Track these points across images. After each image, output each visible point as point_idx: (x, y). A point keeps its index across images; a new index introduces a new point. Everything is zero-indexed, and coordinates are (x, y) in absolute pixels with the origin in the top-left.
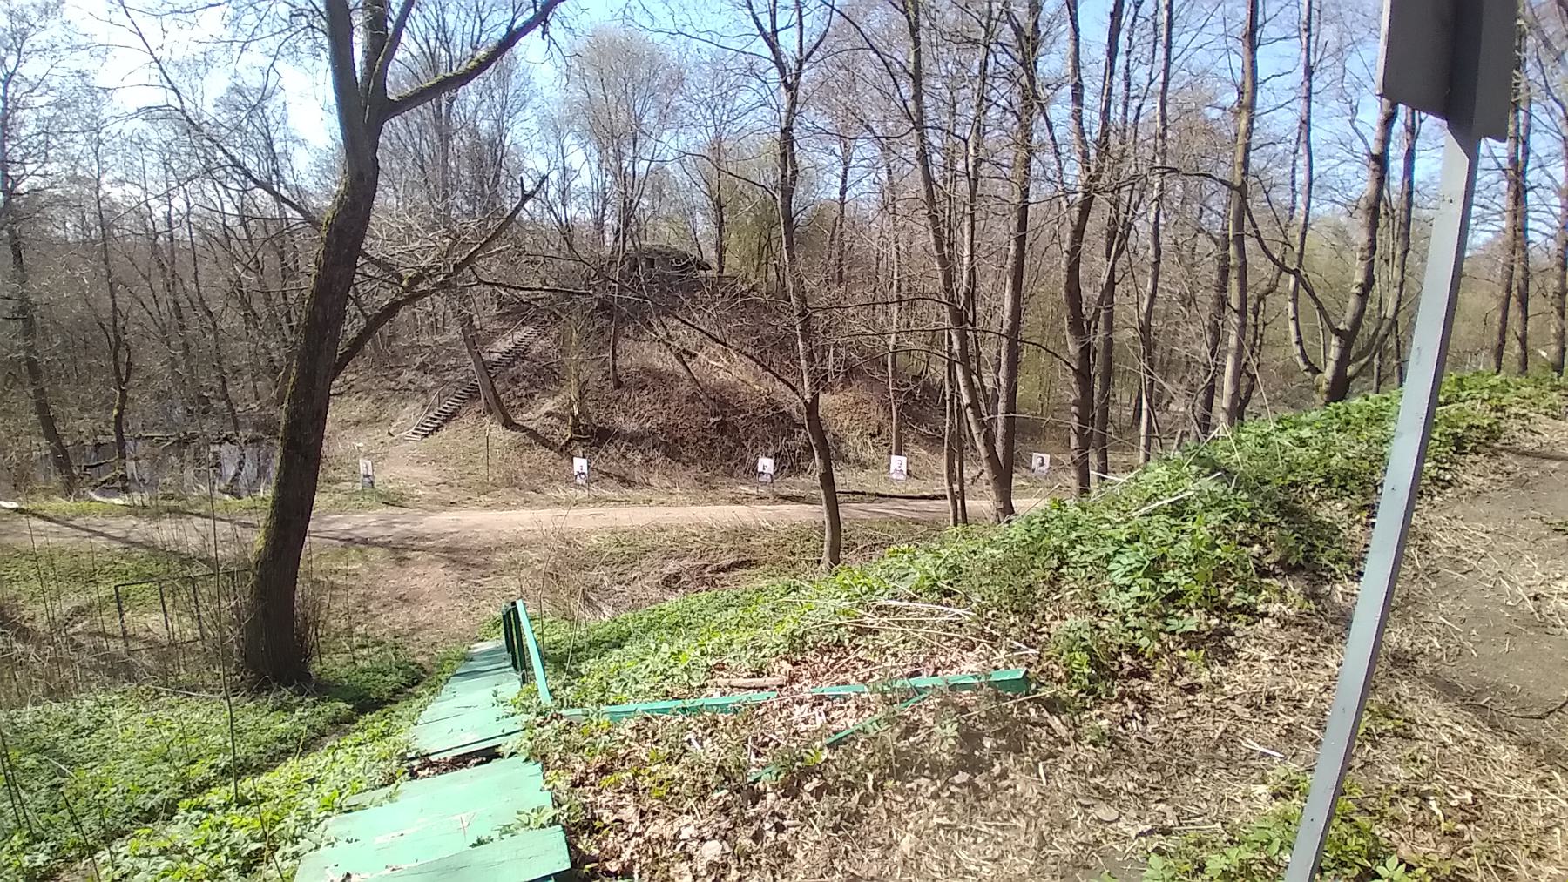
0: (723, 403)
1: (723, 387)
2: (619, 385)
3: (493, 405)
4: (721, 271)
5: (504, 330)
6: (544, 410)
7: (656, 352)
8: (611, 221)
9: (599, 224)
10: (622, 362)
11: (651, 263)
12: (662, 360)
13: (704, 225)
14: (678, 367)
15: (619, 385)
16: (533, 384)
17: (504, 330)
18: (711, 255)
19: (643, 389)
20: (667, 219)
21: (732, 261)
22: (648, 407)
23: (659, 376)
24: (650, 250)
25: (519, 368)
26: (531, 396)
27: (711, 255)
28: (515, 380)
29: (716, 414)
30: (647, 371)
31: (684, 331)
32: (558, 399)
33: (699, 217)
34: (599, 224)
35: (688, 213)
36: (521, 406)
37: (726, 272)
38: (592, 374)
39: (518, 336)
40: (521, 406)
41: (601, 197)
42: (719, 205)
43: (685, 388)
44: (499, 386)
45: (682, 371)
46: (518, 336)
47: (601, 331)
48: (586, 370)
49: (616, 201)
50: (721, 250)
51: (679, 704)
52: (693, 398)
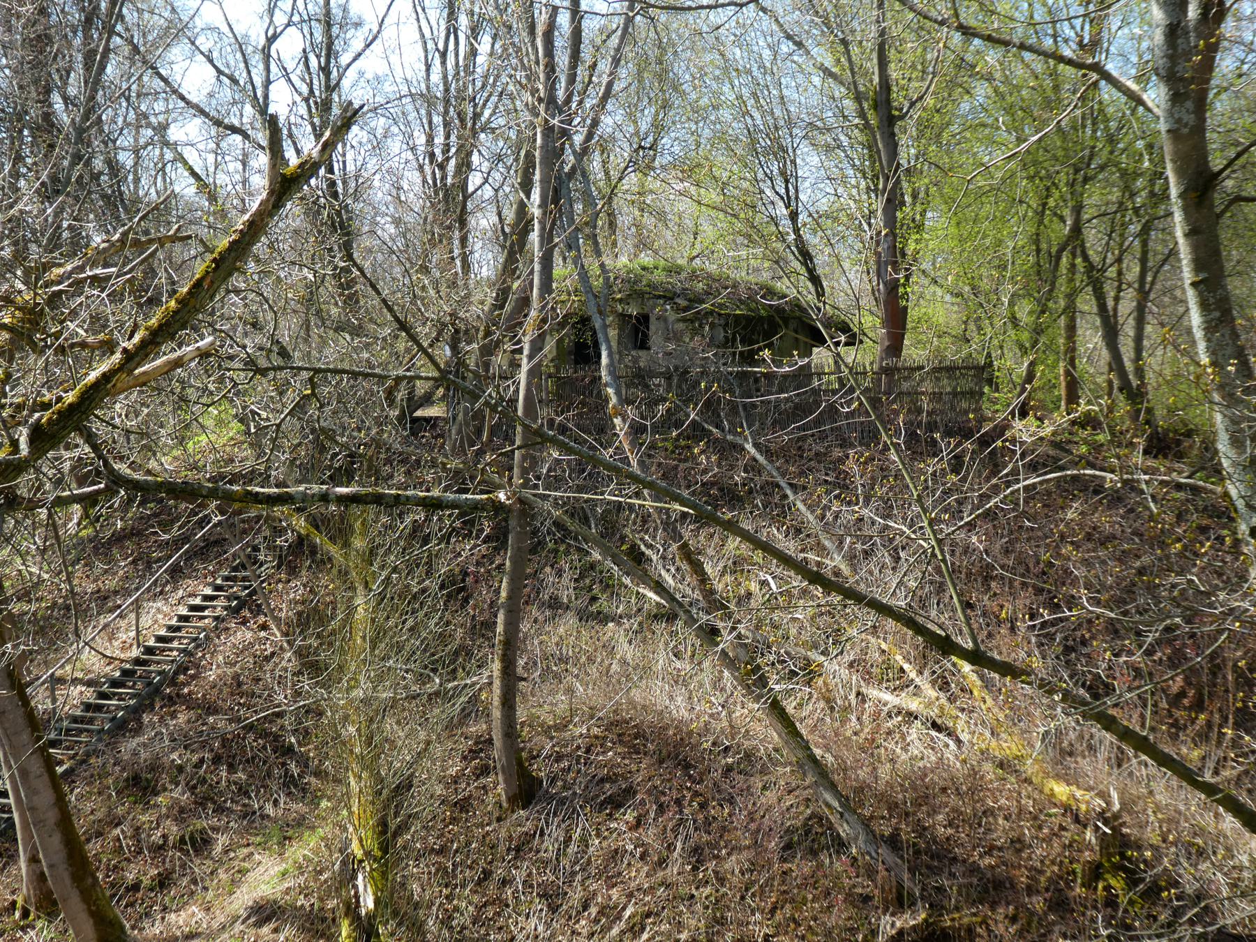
0: (932, 857)
1: (923, 792)
2: (526, 791)
3: (61, 884)
4: (895, 346)
5: (413, 149)
6: (243, 898)
7: (661, 660)
8: (489, 182)
9: (452, 203)
10: (542, 705)
11: (637, 332)
12: (684, 690)
13: (826, 182)
14: (749, 716)
15: (526, 791)
16: (206, 799)
17: (103, 598)
18: (849, 283)
19: (616, 803)
20: (689, 170)
21: (934, 308)
22: (638, 875)
23: (676, 753)
24: (640, 290)
25: (157, 739)
26: (200, 844)
27: (849, 283)
28: (141, 786)
29: (900, 902)
30: (630, 734)
31: (765, 580)
32: (300, 851)
33: (809, 162)
34: (452, 203)
35: (771, 148)
36: (163, 882)
37: (913, 352)
38: (432, 759)
39: (158, 616)
40: (163, 882)
41: (455, 111)
42: (882, 113)
43: (778, 799)
44: (86, 804)
45: (766, 735)
46: (158, 616)
47: (458, 589)
48: (405, 739)
49: (509, 120)
50: (891, 260)
51: (576, 98)
52: (811, 838)
